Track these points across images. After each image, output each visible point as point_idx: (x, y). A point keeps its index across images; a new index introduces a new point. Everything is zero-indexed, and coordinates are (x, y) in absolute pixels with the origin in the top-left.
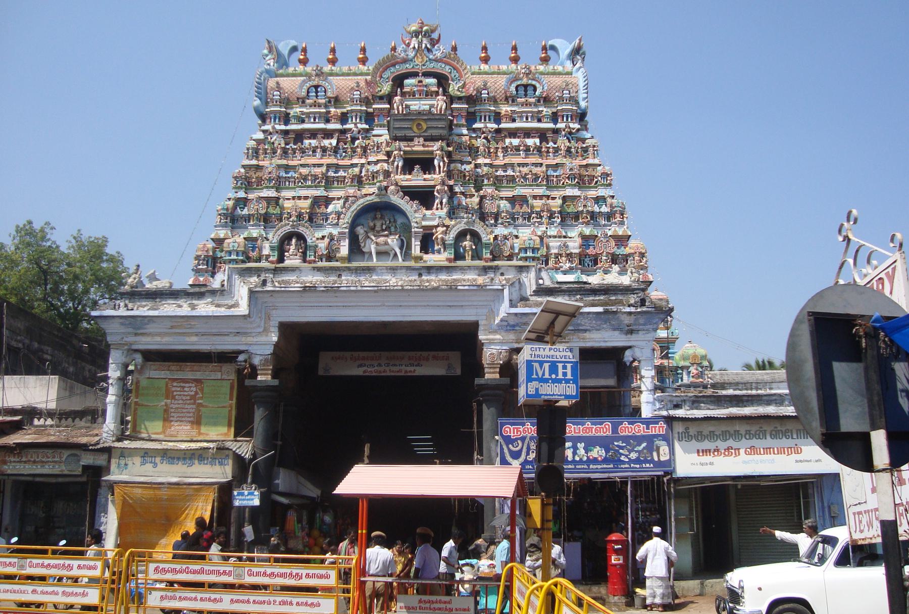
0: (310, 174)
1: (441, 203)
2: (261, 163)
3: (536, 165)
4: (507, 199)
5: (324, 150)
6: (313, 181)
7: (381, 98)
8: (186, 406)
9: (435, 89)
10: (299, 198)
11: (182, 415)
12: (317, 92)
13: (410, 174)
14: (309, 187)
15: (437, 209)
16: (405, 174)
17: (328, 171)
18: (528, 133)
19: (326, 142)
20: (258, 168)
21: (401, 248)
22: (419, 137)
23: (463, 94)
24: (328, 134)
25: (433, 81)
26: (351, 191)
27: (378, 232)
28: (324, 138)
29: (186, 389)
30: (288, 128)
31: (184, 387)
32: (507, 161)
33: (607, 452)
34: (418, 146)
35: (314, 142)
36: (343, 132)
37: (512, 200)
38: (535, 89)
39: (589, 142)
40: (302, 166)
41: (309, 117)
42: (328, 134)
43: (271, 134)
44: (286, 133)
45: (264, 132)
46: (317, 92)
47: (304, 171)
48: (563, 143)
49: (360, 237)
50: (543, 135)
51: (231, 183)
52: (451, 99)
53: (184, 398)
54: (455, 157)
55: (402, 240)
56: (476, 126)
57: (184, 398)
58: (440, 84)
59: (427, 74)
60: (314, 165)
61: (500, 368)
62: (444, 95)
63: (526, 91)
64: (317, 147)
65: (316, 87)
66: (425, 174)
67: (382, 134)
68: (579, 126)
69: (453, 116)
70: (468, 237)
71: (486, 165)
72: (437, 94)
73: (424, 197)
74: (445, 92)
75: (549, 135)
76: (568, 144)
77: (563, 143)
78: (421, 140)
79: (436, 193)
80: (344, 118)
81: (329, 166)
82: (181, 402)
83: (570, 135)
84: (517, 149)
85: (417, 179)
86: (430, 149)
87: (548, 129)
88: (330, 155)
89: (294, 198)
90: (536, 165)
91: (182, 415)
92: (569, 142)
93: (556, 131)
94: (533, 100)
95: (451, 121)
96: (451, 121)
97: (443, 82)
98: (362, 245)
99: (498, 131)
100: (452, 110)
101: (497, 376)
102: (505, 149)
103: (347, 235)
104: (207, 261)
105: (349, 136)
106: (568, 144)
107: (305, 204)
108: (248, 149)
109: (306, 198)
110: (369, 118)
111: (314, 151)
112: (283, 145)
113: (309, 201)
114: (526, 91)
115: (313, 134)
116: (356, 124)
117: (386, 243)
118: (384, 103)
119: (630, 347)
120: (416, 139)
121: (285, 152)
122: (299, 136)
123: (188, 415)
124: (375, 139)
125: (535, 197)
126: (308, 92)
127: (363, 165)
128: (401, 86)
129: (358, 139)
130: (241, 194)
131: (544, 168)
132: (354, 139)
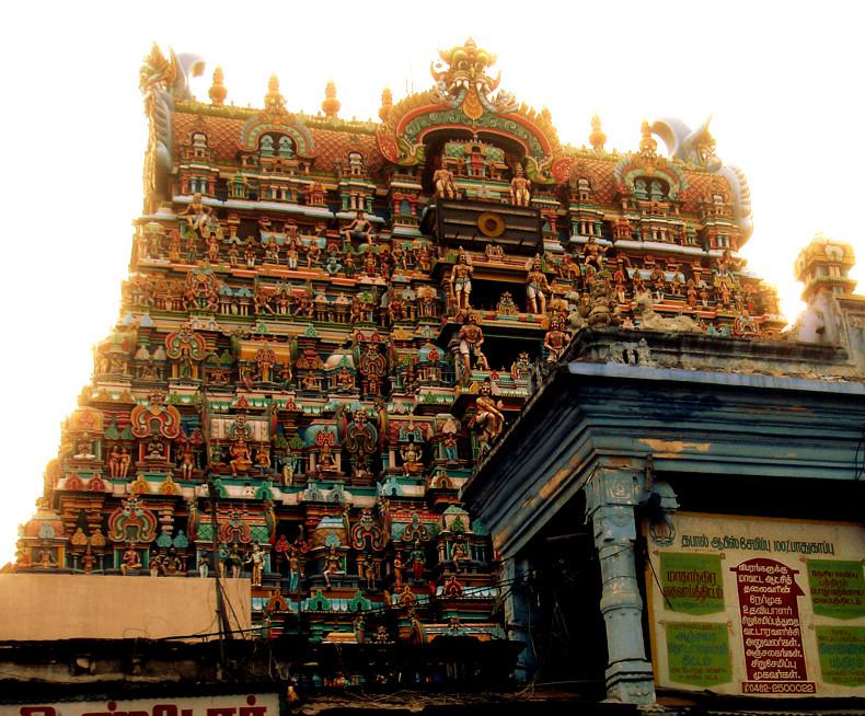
0: (283, 295)
5: (302, 253)
6: (293, 308)
8: (778, 622)
11: (772, 643)
14: (282, 318)
18: (662, 260)
19: (306, 240)
22: (494, 244)
23: (551, 181)
26: (368, 334)
29: (769, 579)
30: (230, 203)
31: (764, 575)
33: (389, 639)
35: (280, 237)
36: (334, 224)
40: (264, 278)
42: (307, 224)
43: (192, 212)
44: (222, 213)
45: (177, 207)
53: (770, 602)
56: (575, 238)
57: (770, 602)
64: (287, 247)
75: (697, 267)
78: (499, 249)
80: (333, 199)
81: (317, 283)
82: (763, 610)
86: (518, 267)
87: (694, 257)
88: (313, 265)
91: (772, 643)
99: (612, 253)
104: (94, 444)
107: (282, 352)
109: (282, 339)
111: (283, 255)
115: (279, 221)
116: (360, 212)
118: (410, 180)
121: (224, 250)
123: (786, 643)
127: (382, 289)
129: (365, 240)
132: (358, 240)
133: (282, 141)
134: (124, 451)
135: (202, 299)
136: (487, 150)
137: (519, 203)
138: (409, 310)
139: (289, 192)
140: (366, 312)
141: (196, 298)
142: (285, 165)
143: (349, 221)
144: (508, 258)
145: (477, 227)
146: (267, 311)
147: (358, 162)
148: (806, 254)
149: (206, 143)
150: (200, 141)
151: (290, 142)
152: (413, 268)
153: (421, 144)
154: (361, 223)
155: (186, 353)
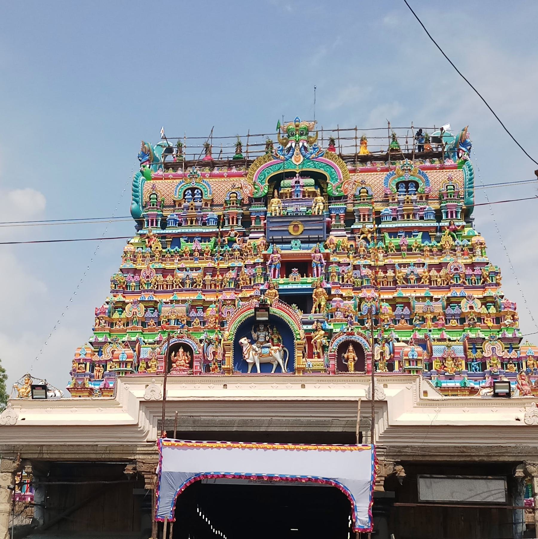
1: (319, 306)
2: (138, 267)
3: (419, 265)
4: (387, 300)
5: (201, 253)
7: (258, 200)
9: (313, 189)
10: (178, 302)
12: (193, 195)
13: (287, 277)
15: (315, 312)
16: (282, 277)
17: (205, 275)
20: (136, 271)
21: (284, 359)
22: (296, 239)
24: (205, 238)
25: (312, 181)
27: (262, 343)
28: (201, 242)
30: (167, 231)
32: (387, 261)
34: (296, 250)
37: (393, 303)
38: (417, 185)
39: (474, 240)
41: (186, 221)
42: (205, 238)
45: (141, 235)
46: (193, 195)
47: (181, 275)
48: (446, 240)
49: (244, 349)
50: (426, 234)
51: (109, 286)
52: (330, 199)
54: (332, 259)
55: (285, 351)
58: (317, 185)
59: (304, 174)
60: (192, 269)
61: (385, 481)
62: (322, 195)
63: (407, 188)
65: (193, 189)
66: (302, 276)
67: (257, 239)
68: (464, 223)
69: (331, 217)
70: (351, 348)
71: (365, 266)
72: (314, 194)
73: (303, 301)
74: (323, 192)
76: (452, 243)
77: (446, 240)
78: (299, 242)
79: (314, 296)
80: (220, 221)
83: (455, 232)
84: (399, 249)
85: (296, 282)
89: (172, 302)
90: (419, 265)
92: (454, 240)
93: (441, 229)
94: (414, 197)
95: (329, 223)
96: (329, 223)
97: (320, 180)
98: (247, 356)
100: (330, 211)
101: (382, 489)
102: (386, 250)
103: (232, 347)
105: (226, 239)
106: (452, 243)
107: (181, 309)
108: (126, 253)
109: (184, 301)
110: (246, 221)
112: (160, 249)
113: (187, 305)
114: (407, 188)
115: (190, 238)
116: (232, 227)
117: (270, 354)
119: (521, 462)
120: (293, 242)
122: (176, 240)
124: (252, 242)
125: (417, 298)
126: (185, 195)
127: (240, 268)
128: (278, 187)
130: (120, 298)
131: (426, 269)
132: (231, 242)
133: (196, 192)
134: (101, 366)
135: (149, 284)
136: (303, 181)
137: (278, 215)
138: (250, 279)
139: (197, 221)
140: (229, 283)
141: (145, 284)
142: (195, 206)
143: (227, 232)
144: (303, 245)
145: (288, 230)
146: (180, 287)
147: (235, 199)
148: (337, 483)
149: (157, 199)
150: (154, 199)
151: (200, 192)
152: (255, 255)
153: (267, 184)
154: (233, 233)
155: (135, 313)
